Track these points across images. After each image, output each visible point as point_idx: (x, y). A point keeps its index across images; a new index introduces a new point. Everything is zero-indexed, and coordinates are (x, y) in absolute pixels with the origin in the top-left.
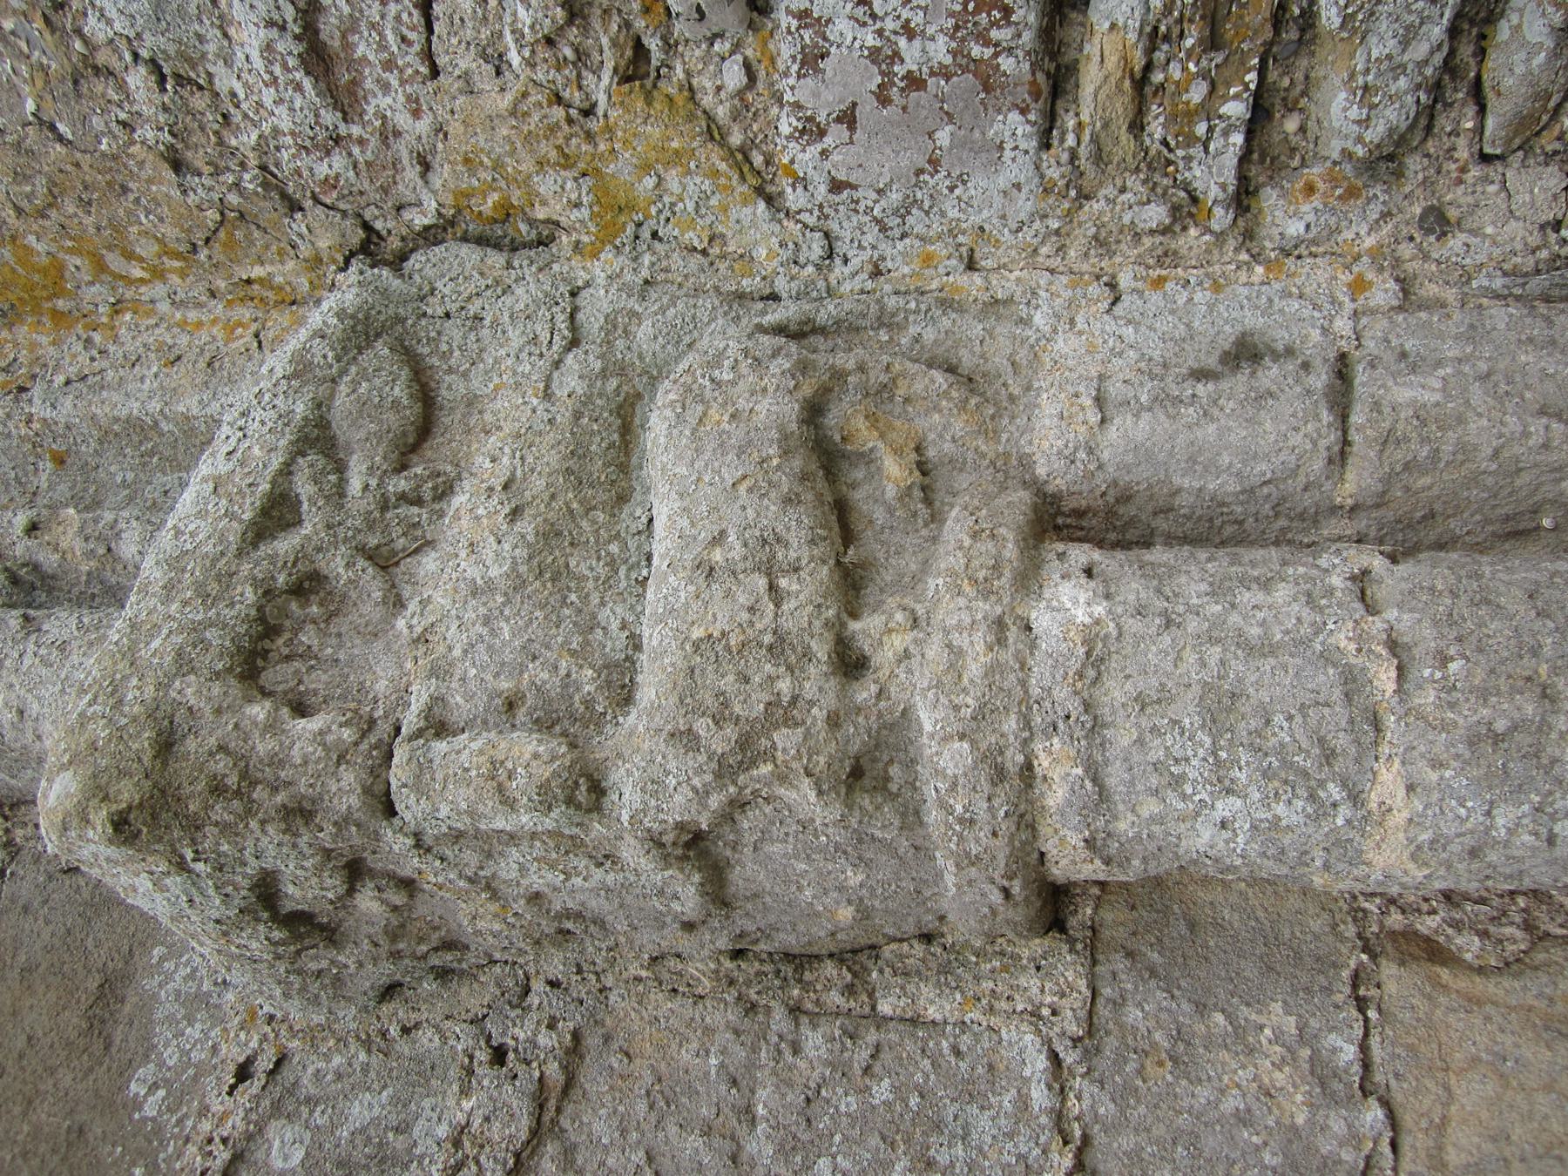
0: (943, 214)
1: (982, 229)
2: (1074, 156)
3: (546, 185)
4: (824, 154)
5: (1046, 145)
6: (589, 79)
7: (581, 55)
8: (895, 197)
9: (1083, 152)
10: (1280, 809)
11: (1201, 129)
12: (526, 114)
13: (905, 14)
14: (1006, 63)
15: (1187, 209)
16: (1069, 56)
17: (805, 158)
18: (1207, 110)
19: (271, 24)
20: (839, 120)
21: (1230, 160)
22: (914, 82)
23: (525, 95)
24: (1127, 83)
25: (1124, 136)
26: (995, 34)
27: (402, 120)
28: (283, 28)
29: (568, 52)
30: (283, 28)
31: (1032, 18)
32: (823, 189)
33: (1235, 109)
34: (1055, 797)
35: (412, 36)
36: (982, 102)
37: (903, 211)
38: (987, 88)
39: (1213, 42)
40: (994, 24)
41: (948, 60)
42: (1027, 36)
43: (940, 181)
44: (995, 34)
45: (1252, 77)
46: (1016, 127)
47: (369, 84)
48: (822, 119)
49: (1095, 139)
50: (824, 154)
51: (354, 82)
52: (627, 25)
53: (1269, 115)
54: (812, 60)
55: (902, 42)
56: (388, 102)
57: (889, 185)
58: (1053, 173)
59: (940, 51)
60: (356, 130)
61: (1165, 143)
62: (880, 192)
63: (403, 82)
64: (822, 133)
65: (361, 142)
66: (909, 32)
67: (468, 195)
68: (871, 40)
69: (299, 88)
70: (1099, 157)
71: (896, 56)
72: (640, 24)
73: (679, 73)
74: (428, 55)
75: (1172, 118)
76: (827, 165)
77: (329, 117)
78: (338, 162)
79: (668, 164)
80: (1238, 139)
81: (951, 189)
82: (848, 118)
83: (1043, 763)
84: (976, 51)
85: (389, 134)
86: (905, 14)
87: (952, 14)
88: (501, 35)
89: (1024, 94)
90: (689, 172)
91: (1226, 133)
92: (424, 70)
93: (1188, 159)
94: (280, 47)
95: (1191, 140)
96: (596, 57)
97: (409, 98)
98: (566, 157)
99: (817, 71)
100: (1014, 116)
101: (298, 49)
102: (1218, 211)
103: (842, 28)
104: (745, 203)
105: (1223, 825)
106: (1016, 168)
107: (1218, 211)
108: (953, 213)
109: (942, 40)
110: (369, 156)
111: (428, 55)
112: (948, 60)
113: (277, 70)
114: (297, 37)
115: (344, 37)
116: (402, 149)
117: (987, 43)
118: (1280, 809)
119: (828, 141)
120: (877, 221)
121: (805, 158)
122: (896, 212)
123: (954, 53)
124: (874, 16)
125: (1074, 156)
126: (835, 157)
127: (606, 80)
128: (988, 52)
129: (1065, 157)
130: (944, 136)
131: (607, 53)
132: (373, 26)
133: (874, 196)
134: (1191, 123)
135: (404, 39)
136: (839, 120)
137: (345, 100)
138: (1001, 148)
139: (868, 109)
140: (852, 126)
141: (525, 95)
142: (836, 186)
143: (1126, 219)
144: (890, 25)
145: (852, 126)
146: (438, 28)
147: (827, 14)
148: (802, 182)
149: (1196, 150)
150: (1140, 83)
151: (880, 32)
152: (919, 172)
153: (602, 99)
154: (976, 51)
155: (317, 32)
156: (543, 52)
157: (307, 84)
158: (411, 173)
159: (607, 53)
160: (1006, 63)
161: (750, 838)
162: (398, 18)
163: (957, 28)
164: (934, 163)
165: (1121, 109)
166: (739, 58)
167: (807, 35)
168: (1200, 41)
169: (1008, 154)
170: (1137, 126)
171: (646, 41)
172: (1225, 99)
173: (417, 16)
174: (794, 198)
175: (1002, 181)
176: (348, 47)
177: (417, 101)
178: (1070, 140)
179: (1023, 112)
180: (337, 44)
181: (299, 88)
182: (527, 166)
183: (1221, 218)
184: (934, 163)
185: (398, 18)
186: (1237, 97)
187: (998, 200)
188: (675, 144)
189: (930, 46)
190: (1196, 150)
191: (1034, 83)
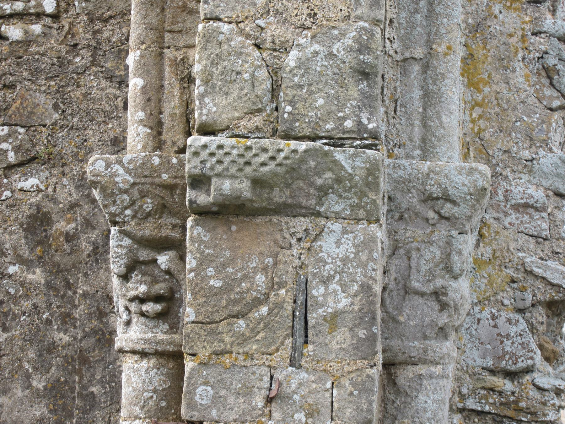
0: (468, 343)
1: (465, 352)
2: (481, 374)
3: (489, 250)
4: (488, 319)
5: (483, 368)
6: (513, 270)
7: (517, 269)
8: (474, 333)
9: (481, 376)
10: (430, 412)
11: (483, 401)
12: (508, 252)
13: (517, 343)
14: (504, 362)
15: (463, 397)
16: (497, 374)
17: (486, 314)
18: (487, 403)
19: (537, 201)
20: (496, 324)
21: (474, 407)
22: (502, 342)
23: (512, 254)
24: (493, 386)
25: (481, 385)
26: (511, 361)
27: (509, 219)
28: (536, 202)
29: (519, 267)
30: (536, 202)
31: (512, 369)
32: (479, 316)
33: (487, 408)
34: (433, 369)
35: (527, 230)
36: (495, 356)
37: (472, 336)
38: (499, 358)
39: (502, 404)
40: (513, 361)
41: (506, 350)
42: (509, 367)
43: (477, 343)
44: (511, 361)
45: (493, 411)
46: (490, 363)
47: (518, 215)
48: (497, 320)
49: (483, 379)
50: (488, 319)
51: (519, 211)
52: (521, 281)
53: (479, 415)
54: (509, 321)
55: (511, 341)
56: (513, 217)
57: (477, 332)
58: (476, 370)
59: (508, 349)
60: (508, 206)
61: (479, 394)
62: (476, 330)
63: (518, 224)
64: (493, 320)
65: (505, 206)
66: (513, 343)
67: (489, 228)
68: (512, 335)
69: (522, 199)
70: (479, 379)
71: (508, 339)
72: (521, 284)
73: (508, 289)
74: (522, 232)
75: (485, 395)
76: (485, 319)
77: (513, 202)
78: (501, 198)
79: (489, 281)
80: (479, 409)
81: (475, 346)
82: (495, 326)
83: (439, 367)
84: (507, 357)
85: (506, 214)
86: (517, 343)
87: (516, 353)
88: (525, 252)
89: (497, 365)
90: (486, 285)
91: (480, 406)
92: (520, 230)
93: (475, 398)
94: (532, 200)
95: (480, 399)
96: (516, 272)
97: (514, 224)
98: (496, 258)
99: (507, 322)
100: (492, 363)
101: (531, 203)
102: (462, 405)
103: (515, 329)
104: (477, 297)
105: (426, 402)
106: (479, 362)
107: (462, 405)
108: (469, 346)
109: (511, 350)
110: (502, 206)
111: (522, 232)
112: (506, 350)
113: (527, 196)
114: (533, 204)
115: (529, 214)
116: (501, 215)
117: (509, 359)
118: (430, 412)
119: (491, 321)
120: (469, 328)
121: (486, 314)
122: (471, 332)
123: (507, 352)
124: (517, 336)
125: (479, 374)
126: (487, 321)
127: (512, 274)
128: (507, 359)
129: (480, 372)
130: (489, 347)
131: (517, 276)
132: (530, 222)
133: (475, 328)
134: (485, 399)
135: (526, 228)
136: (496, 324)
137: (517, 207)
138: (484, 358)
139: (496, 330)
140: (493, 327)
141: (512, 254)
142: (479, 320)
143: (465, 385)
144: (515, 339)
145: (493, 327)
146: (527, 236)
147: (518, 326)
148: (481, 312)
149: (477, 400)
150: (492, 390)
151: (513, 337)
152: (479, 339)
153: (508, 271)
154: (507, 357)
155: (532, 208)
156: (521, 262)
157: (523, 202)
158: (495, 215)
159: (517, 276)
160: (504, 362)
161: (429, 303)
162: (531, 229)
163: (513, 353)
164: (482, 343)
165: (488, 385)
166: (509, 304)
167: (514, 321)
168: (502, 401)
169: (483, 360)
170: (483, 388)
171: (516, 284)
172: (489, 406)
173: (531, 233)
174: (477, 309)
175: (476, 358)
176: (527, 214)
177: (513, 226)
178: (484, 374)
179: (493, 365)
180: (528, 211)
181: (522, 199)
182: (494, 247)
183: (460, 405)
184: (482, 343)
185: (531, 229)
186: (490, 408)
187: (472, 357)
188: (494, 285)
189: (509, 347)
190: (477, 400)
191: (498, 367)
